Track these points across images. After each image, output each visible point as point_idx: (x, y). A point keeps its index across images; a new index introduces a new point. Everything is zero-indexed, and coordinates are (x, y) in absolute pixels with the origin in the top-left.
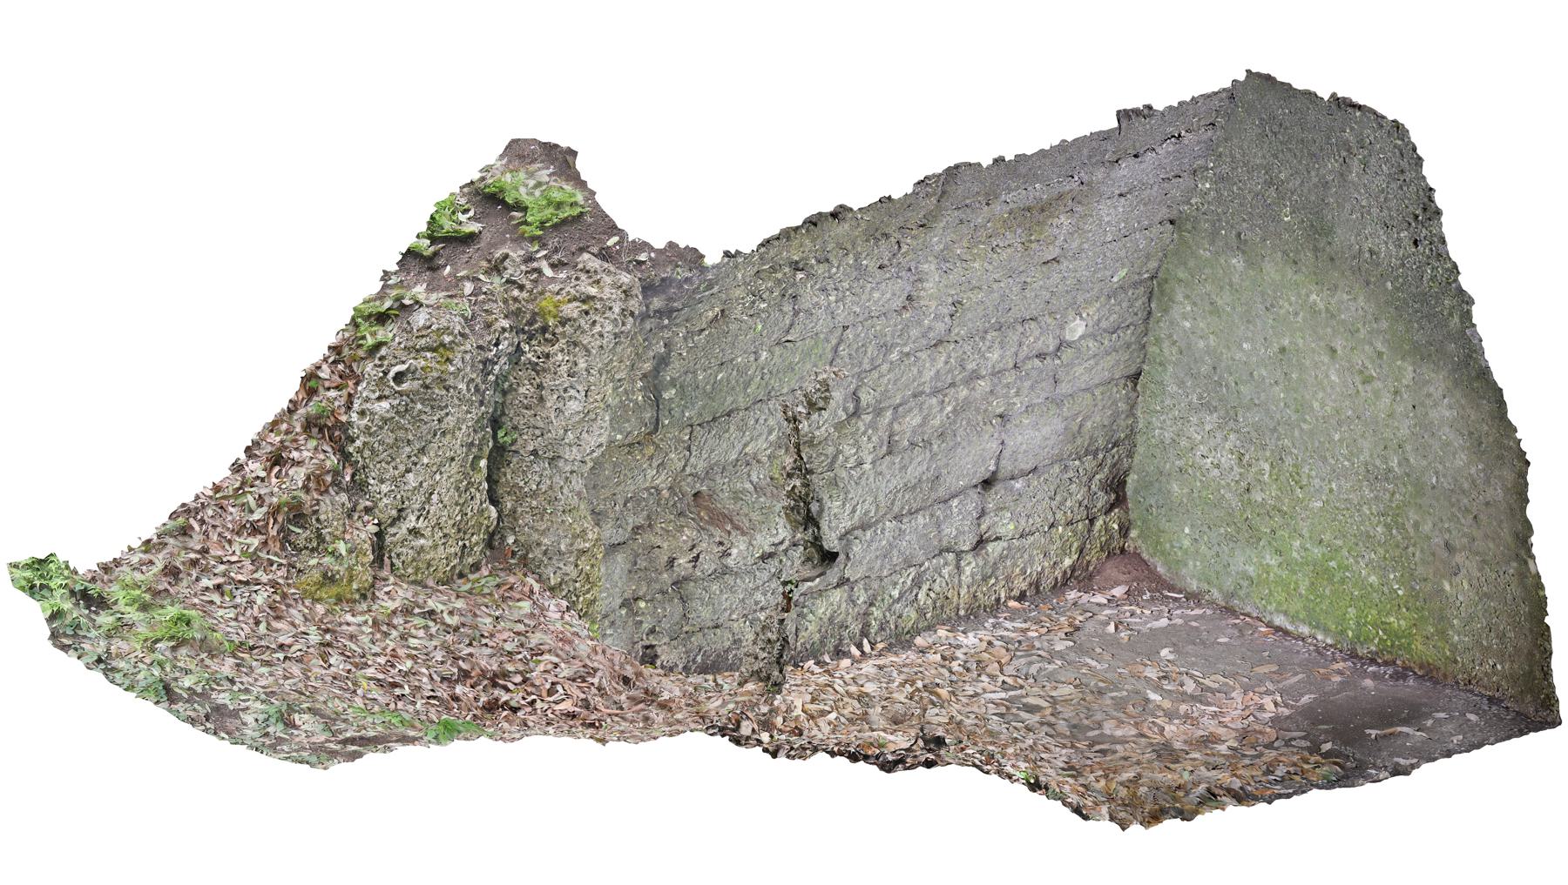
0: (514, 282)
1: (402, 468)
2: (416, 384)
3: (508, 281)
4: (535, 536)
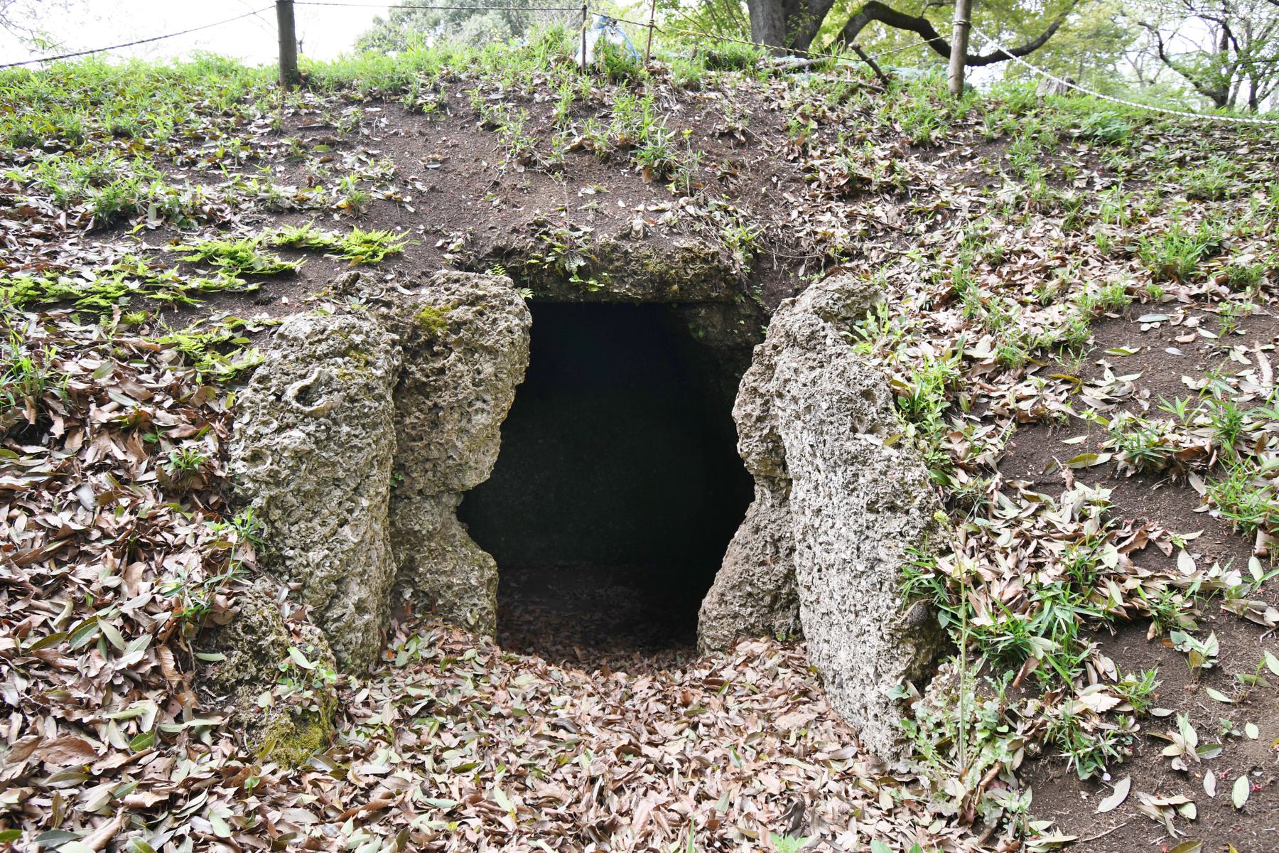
0: (376, 302)
1: (333, 522)
2: (337, 397)
3: (367, 302)
4: (443, 579)
